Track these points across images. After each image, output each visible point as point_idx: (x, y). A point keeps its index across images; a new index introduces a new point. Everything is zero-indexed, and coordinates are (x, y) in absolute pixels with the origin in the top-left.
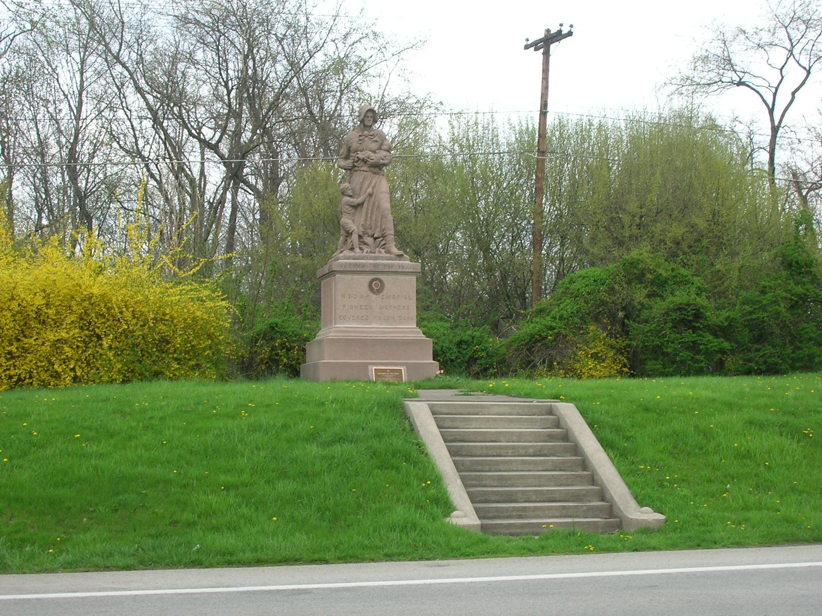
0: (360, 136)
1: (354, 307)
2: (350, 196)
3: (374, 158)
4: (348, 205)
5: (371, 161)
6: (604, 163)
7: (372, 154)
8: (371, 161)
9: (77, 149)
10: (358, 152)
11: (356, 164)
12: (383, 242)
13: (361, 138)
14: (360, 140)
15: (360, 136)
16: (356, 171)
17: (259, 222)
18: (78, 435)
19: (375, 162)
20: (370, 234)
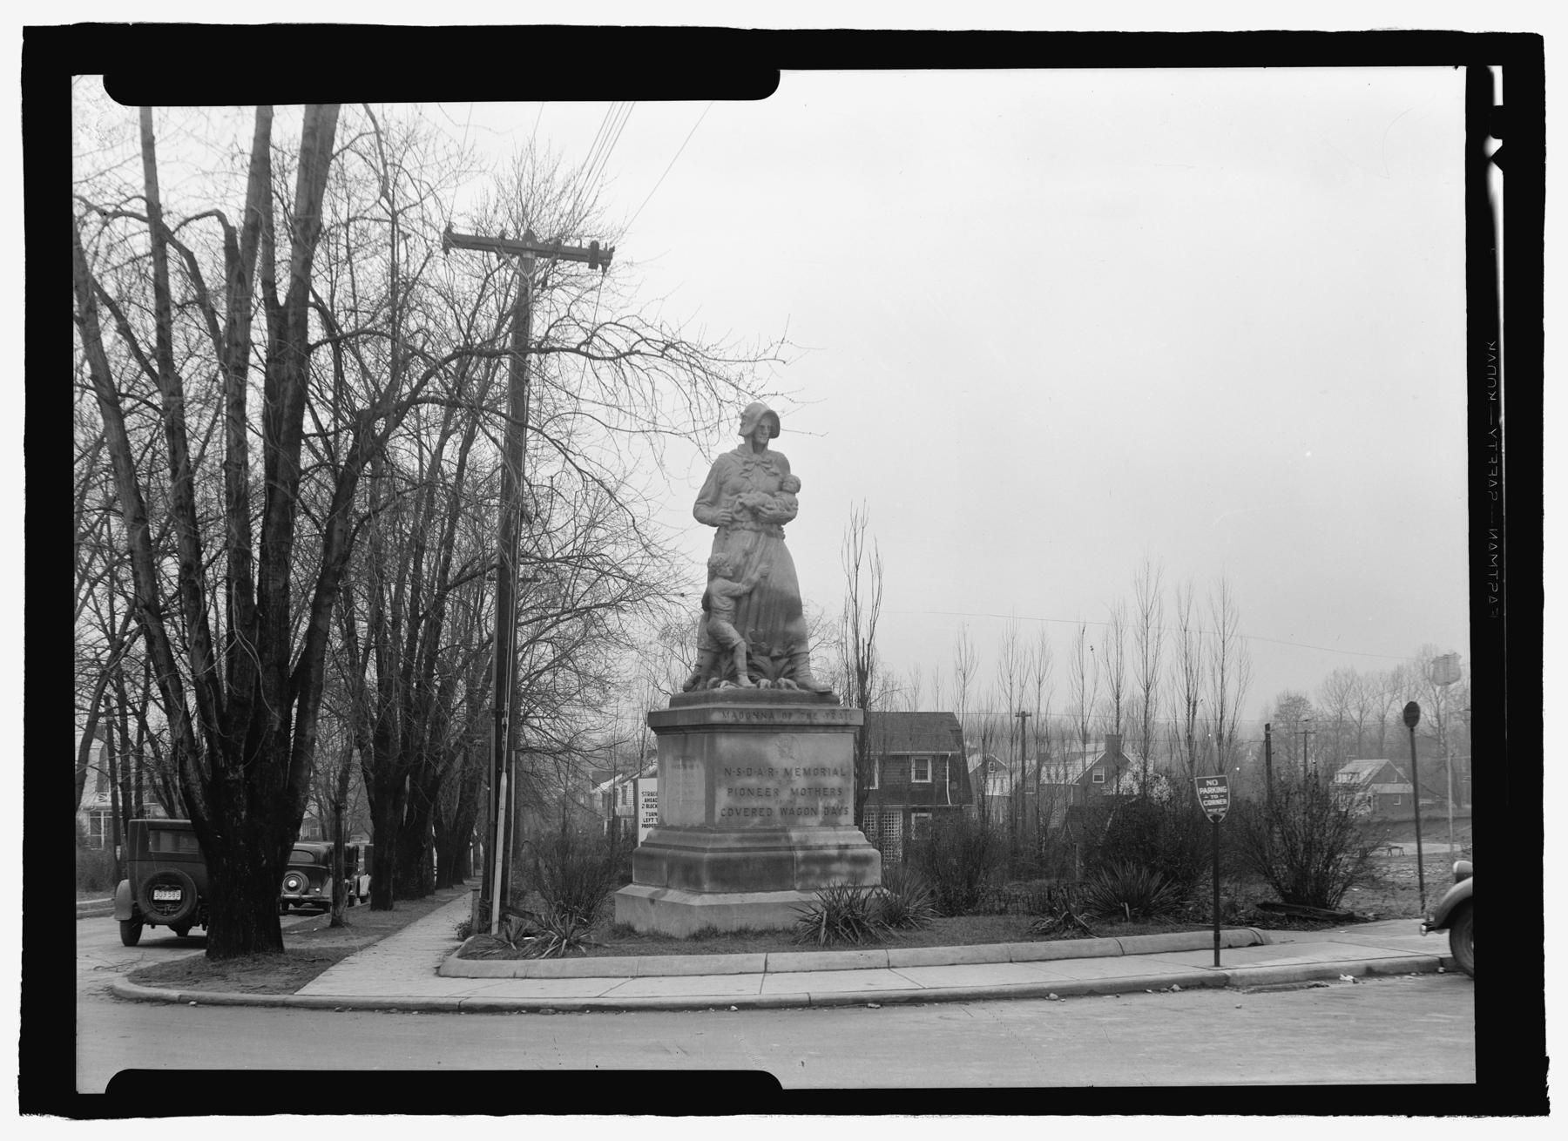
0: (746, 463)
1: (756, 792)
2: (730, 579)
3: (775, 506)
4: (724, 595)
5: (769, 512)
6: (729, 644)
7: (770, 498)
8: (769, 512)
9: (310, 707)
10: (742, 494)
11: (736, 516)
12: (788, 668)
13: (747, 467)
14: (746, 470)
15: (746, 463)
16: (737, 529)
17: (439, 692)
18: (279, 849)
19: (775, 515)
20: (765, 651)
